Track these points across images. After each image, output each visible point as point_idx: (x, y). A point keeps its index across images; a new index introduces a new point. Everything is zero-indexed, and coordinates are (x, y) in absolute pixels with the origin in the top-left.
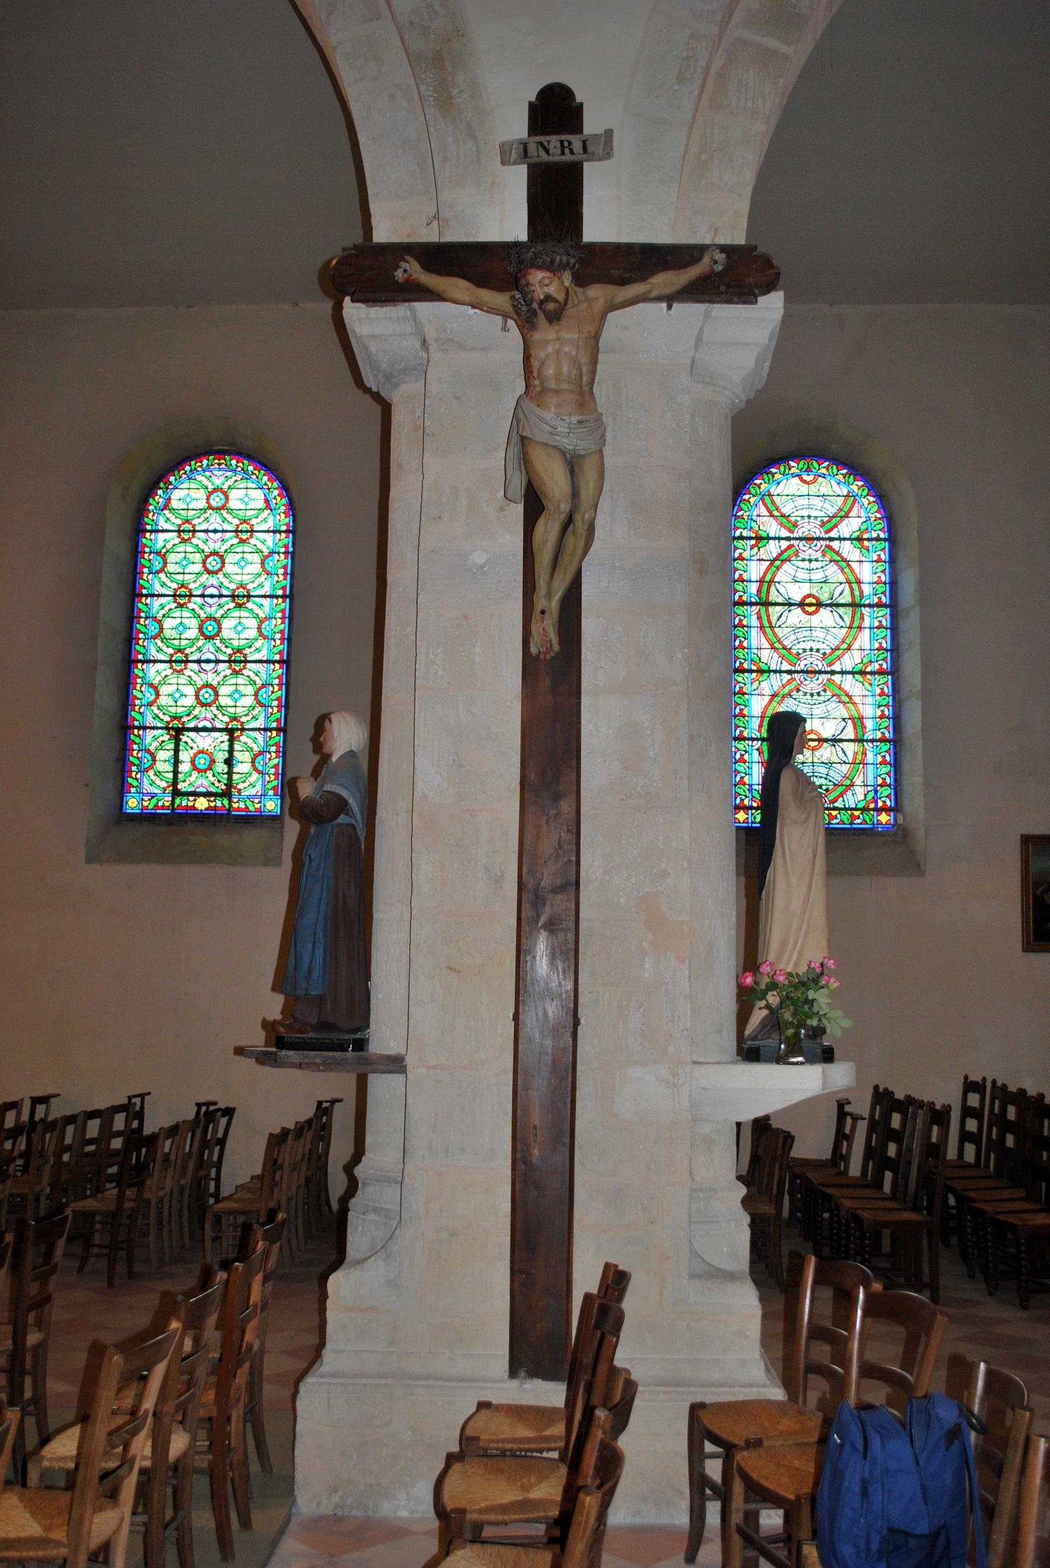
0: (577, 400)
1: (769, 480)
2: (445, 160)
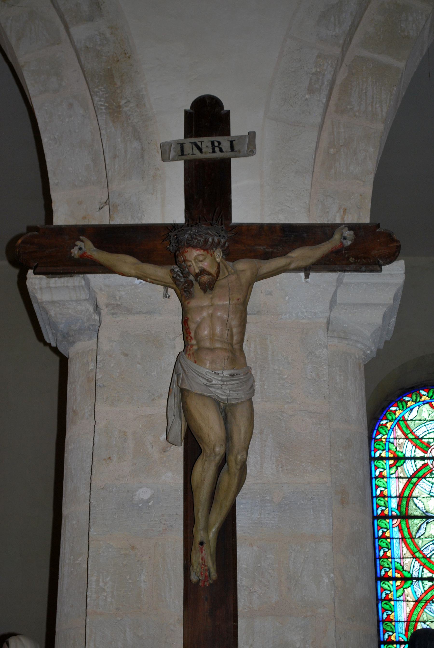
0: (229, 357)
1: (403, 407)
2: (115, 157)
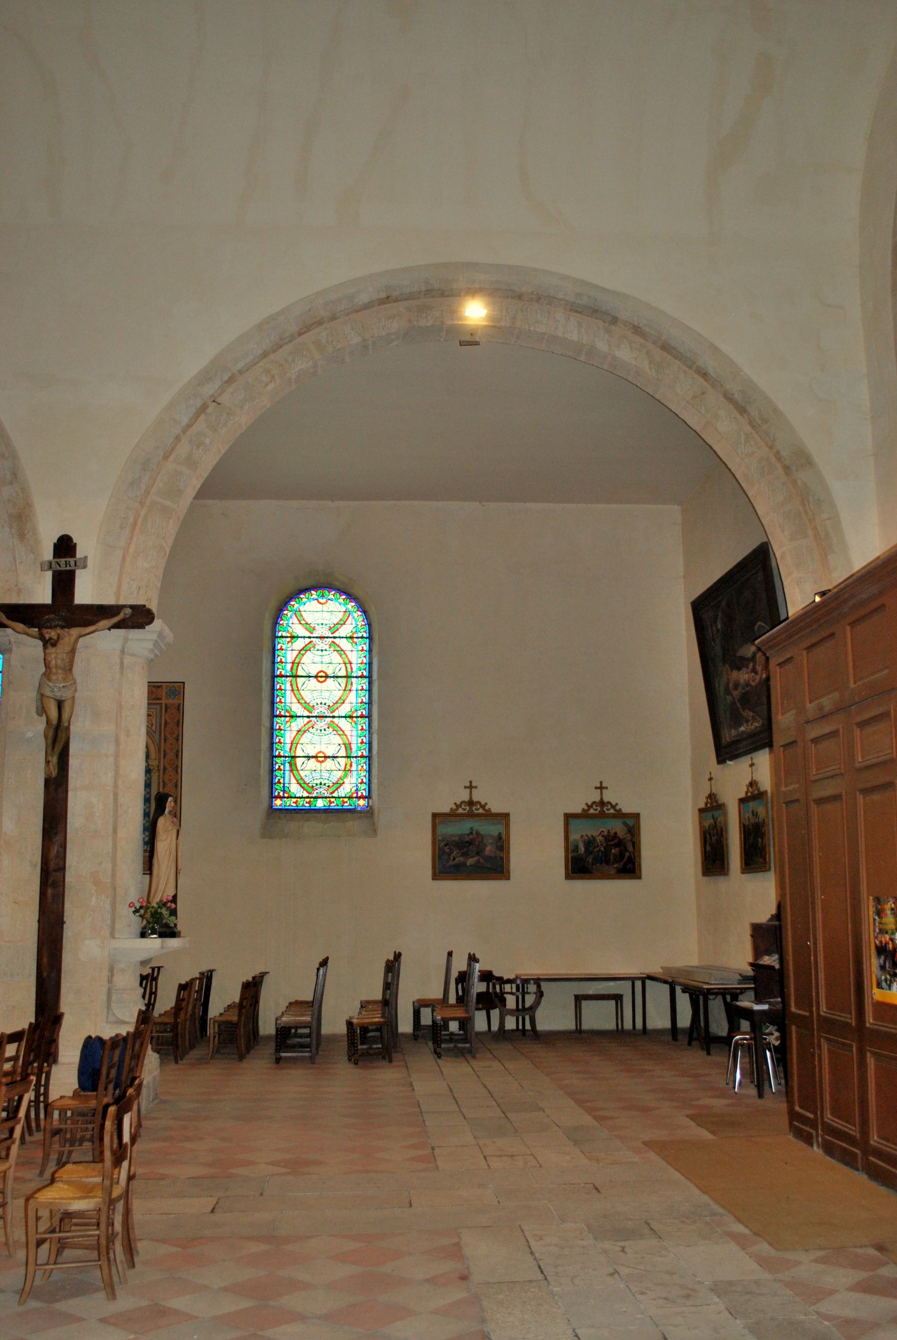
2: (21, 562)
